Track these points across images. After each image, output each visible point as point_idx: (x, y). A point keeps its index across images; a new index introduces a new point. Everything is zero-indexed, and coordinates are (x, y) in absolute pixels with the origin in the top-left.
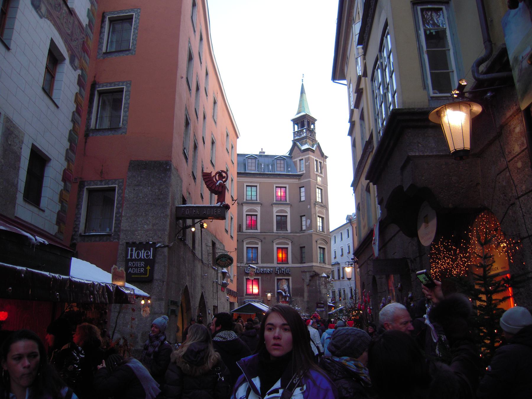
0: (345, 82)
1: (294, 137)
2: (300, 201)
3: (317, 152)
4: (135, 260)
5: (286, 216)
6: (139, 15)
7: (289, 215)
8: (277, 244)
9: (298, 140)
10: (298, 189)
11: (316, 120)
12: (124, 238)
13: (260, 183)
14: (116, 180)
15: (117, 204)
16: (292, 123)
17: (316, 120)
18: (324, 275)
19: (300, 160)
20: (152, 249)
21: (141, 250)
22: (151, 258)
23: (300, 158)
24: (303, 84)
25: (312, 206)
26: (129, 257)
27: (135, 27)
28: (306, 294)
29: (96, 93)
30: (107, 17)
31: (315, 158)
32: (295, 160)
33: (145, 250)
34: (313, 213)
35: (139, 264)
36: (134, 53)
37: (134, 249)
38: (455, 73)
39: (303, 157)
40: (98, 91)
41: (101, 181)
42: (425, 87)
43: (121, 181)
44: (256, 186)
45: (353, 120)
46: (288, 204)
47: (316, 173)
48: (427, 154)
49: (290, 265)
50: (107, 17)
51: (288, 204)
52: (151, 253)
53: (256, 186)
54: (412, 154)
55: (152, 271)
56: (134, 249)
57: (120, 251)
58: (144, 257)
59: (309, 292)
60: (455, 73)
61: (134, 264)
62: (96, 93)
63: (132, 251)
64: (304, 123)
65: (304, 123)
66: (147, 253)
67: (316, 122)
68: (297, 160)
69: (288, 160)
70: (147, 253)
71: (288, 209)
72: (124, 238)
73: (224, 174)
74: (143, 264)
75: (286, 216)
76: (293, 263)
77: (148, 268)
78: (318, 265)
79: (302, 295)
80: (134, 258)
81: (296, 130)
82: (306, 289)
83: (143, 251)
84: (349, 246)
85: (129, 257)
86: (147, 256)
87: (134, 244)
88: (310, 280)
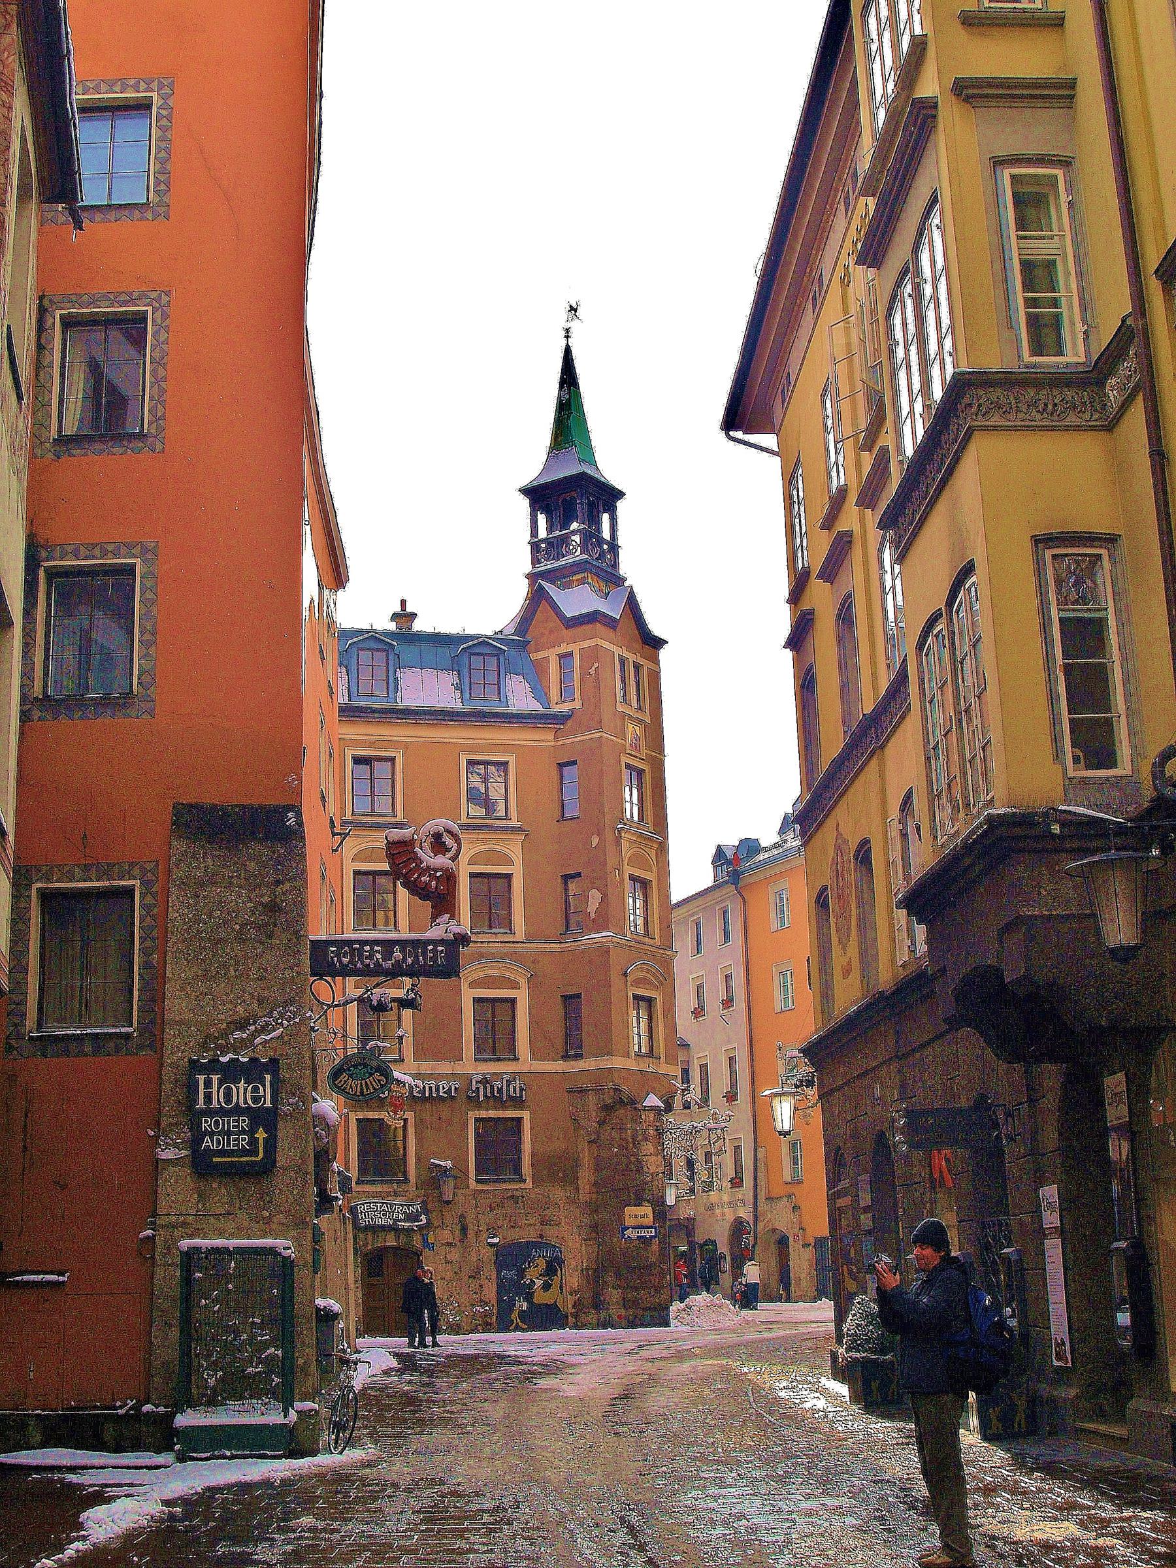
0: (768, 440)
1: (535, 561)
2: (563, 818)
3: (629, 627)
4: (222, 1112)
5: (509, 876)
6: (165, 316)
7: (517, 871)
8: (474, 985)
9: (549, 575)
10: (555, 773)
11: (619, 495)
12: (178, 1048)
13: (406, 747)
14: (132, 864)
15: (143, 940)
16: (524, 503)
17: (619, 495)
18: (653, 1101)
19: (561, 657)
20: (268, 1077)
21: (236, 1081)
22: (268, 1104)
23: (563, 649)
24: (568, 352)
25: (610, 836)
26: (201, 1104)
27: (157, 355)
28: (586, 1177)
29: (42, 573)
30: (58, 313)
31: (618, 651)
32: (542, 654)
33: (248, 1082)
34: (611, 862)
35: (231, 1122)
36: (159, 447)
37: (215, 1078)
38: (1123, 719)
39: (575, 648)
40: (47, 569)
41: (87, 868)
42: (1058, 756)
43: (149, 866)
44: (392, 760)
45: (805, 605)
46: (513, 829)
47: (620, 708)
48: (1059, 911)
49: (526, 1063)
50: (58, 313)
51: (513, 829)
52: (266, 1091)
53: (392, 760)
54: (1025, 912)
55: (271, 1145)
56: (215, 1078)
57: (167, 1087)
58: (245, 1102)
59: (598, 1166)
60: (1123, 719)
61: (217, 1122)
62: (42, 573)
63: (208, 1084)
64: (572, 500)
65: (572, 500)
66: (255, 1089)
67: (620, 504)
68: (552, 654)
69: (512, 652)
70: (255, 1089)
71: (515, 850)
72: (178, 1048)
73: (449, 841)
74: (244, 1123)
75: (509, 876)
76: (533, 1056)
77: (261, 1134)
78: (629, 1064)
79: (570, 1178)
80: (215, 1104)
81: (542, 533)
82: (586, 1158)
83: (242, 1085)
84: (728, 977)
85: (201, 1104)
86: (256, 1100)
87: (213, 1066)
88: (601, 1123)
